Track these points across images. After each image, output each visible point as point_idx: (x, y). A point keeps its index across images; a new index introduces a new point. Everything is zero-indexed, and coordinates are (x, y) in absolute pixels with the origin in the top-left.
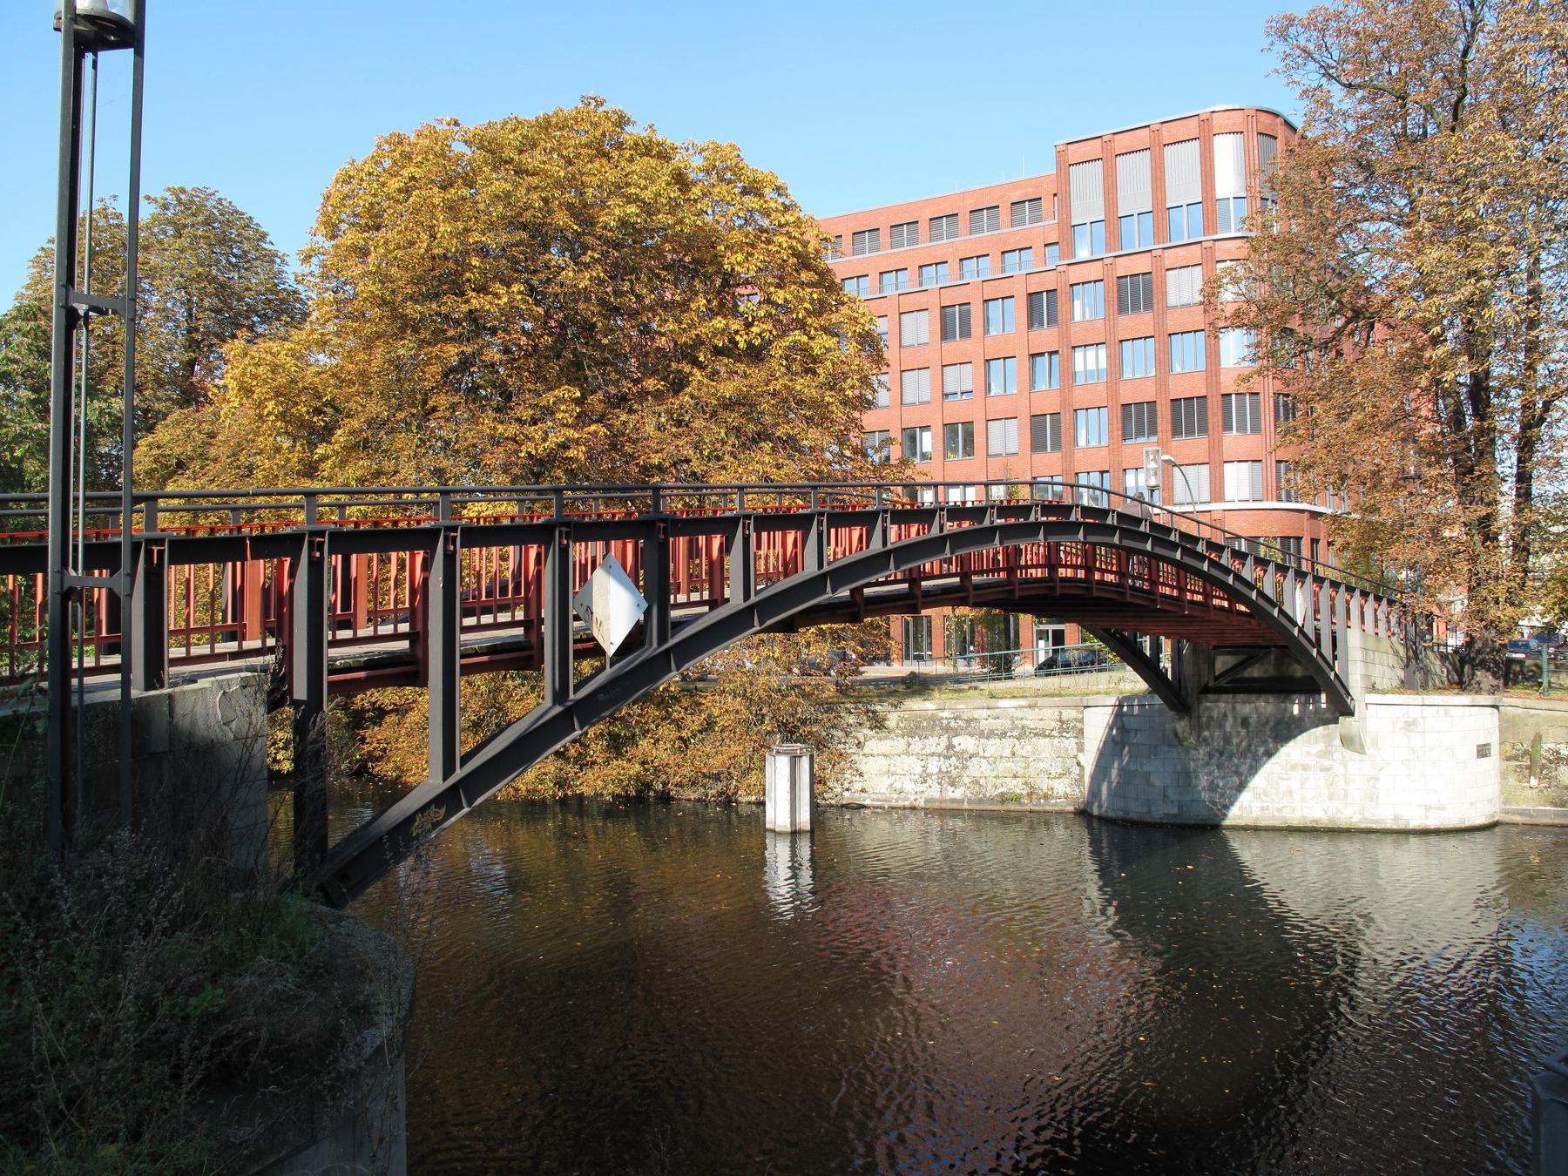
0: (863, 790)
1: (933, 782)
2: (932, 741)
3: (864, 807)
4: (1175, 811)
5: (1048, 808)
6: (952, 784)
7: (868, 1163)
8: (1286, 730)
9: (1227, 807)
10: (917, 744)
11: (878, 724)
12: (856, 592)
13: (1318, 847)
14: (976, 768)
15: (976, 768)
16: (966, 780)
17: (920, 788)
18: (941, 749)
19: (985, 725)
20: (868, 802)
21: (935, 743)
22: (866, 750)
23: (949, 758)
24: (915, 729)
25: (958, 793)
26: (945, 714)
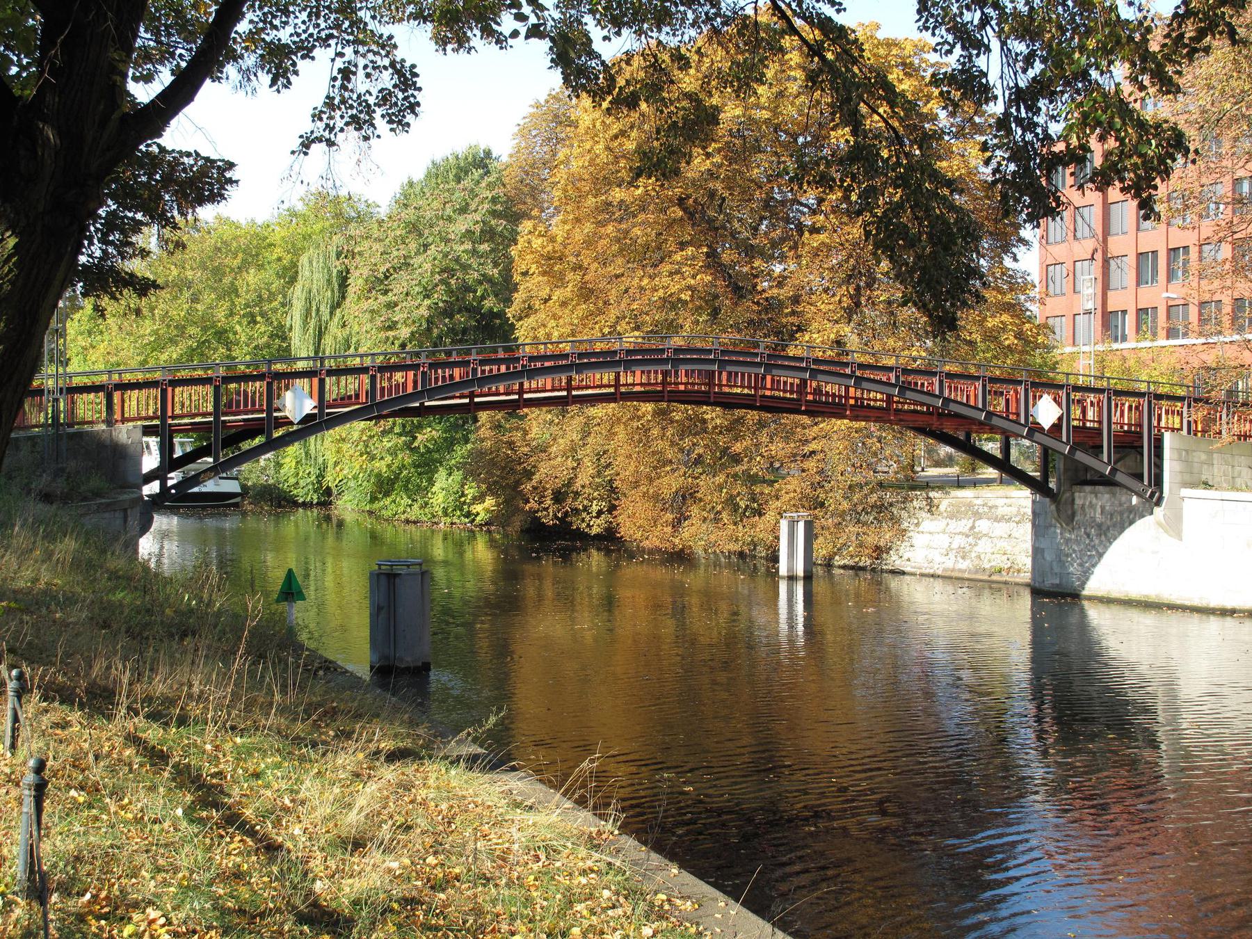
0: (909, 560)
1: (952, 555)
2: (964, 522)
3: (903, 573)
4: (1057, 581)
5: (1017, 580)
6: (963, 558)
7: (239, 528)
8: (1122, 521)
9: (1084, 583)
10: (953, 524)
11: (931, 506)
12: (422, 404)
13: (1147, 620)
14: (984, 546)
15: (984, 546)
16: (973, 555)
17: (944, 559)
18: (966, 530)
19: (1000, 512)
20: (907, 569)
21: (964, 525)
22: (921, 529)
23: (967, 536)
24: (953, 515)
25: (963, 565)
26: (979, 502)
